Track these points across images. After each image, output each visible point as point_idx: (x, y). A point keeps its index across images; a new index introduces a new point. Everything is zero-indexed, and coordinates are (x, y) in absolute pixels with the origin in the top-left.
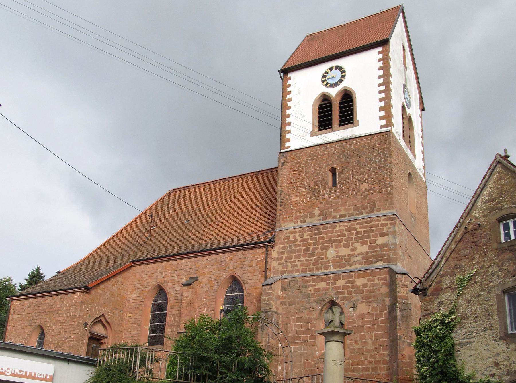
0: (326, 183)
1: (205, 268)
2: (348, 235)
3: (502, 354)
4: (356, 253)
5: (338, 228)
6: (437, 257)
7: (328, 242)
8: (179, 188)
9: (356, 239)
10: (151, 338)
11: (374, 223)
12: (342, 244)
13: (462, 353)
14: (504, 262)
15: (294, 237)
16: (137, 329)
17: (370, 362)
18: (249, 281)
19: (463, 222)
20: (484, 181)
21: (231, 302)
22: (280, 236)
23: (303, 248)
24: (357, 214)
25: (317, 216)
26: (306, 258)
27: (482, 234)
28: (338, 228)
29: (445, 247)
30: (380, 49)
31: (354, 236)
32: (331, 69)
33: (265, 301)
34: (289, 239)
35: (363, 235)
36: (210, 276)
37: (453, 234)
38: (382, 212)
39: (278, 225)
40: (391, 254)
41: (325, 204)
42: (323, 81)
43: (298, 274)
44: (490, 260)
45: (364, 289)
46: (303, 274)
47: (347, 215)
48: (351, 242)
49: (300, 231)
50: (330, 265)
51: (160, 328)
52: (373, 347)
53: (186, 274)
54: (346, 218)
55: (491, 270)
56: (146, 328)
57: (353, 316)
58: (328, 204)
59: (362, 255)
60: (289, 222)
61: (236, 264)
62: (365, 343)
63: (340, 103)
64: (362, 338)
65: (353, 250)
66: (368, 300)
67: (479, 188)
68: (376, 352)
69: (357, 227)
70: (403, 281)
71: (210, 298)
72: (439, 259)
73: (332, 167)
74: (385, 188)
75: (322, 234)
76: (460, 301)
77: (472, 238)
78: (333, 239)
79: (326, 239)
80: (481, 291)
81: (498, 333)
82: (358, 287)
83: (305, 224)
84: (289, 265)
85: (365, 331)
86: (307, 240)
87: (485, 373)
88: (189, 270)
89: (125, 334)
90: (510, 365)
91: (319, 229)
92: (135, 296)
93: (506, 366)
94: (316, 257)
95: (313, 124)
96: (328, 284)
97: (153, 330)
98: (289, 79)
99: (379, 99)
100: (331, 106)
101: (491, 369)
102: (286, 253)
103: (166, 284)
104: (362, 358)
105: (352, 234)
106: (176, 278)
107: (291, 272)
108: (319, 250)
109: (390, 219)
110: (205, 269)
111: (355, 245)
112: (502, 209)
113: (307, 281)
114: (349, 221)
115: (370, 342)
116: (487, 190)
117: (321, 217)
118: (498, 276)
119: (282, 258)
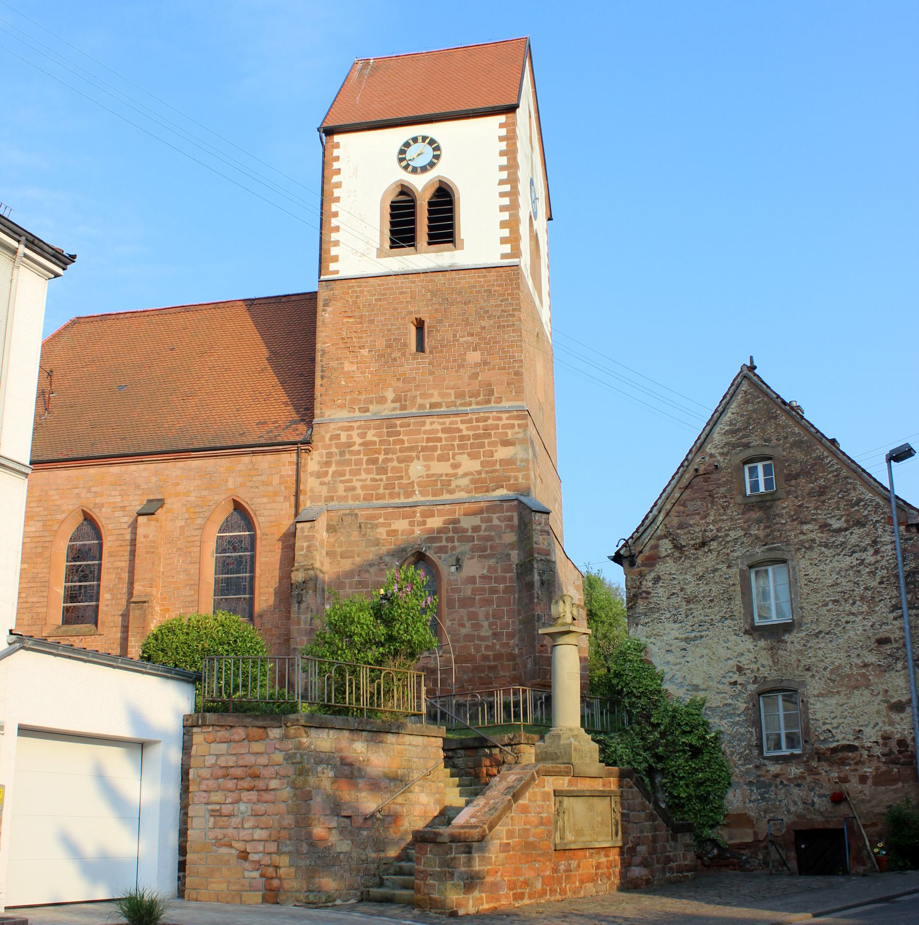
0: (405, 345)
1: (178, 484)
2: (447, 439)
3: (746, 654)
4: (460, 471)
5: (428, 427)
6: (652, 508)
7: (412, 449)
8: (89, 315)
9: (460, 447)
10: (66, 610)
11: (490, 422)
12: (436, 454)
13: (690, 653)
14: (752, 524)
15: (350, 437)
16: (41, 594)
17: (485, 658)
18: (266, 513)
19: (693, 459)
20: (724, 402)
21: (229, 548)
22: (323, 433)
23: (365, 458)
24: (462, 405)
25: (389, 401)
26: (372, 476)
27: (720, 480)
28: (428, 427)
29: (664, 495)
30: (502, 118)
31: (456, 443)
32: (415, 140)
33: (302, 550)
34: (340, 439)
35: (472, 441)
36: (189, 499)
37: (677, 476)
38: (505, 404)
39: (317, 412)
40: (520, 476)
41: (404, 382)
42: (401, 160)
43: (357, 502)
44: (732, 519)
45: (475, 535)
46: (366, 504)
47: (444, 405)
48: (451, 453)
49: (359, 428)
50: (415, 491)
51: (85, 592)
52: (491, 632)
53: (139, 492)
54: (443, 409)
55: (733, 534)
57: (456, 580)
58: (409, 383)
59: (471, 477)
60: (338, 409)
61: (240, 480)
62: (477, 626)
63: (430, 204)
64: (473, 616)
65: (456, 466)
66: (481, 552)
67: (716, 411)
68: (495, 641)
69: (462, 426)
70: (543, 525)
71: (189, 539)
72: (655, 512)
73: (418, 316)
74: (510, 363)
75: (399, 435)
76: (688, 577)
77: (705, 484)
78: (420, 444)
79: (406, 445)
80: (718, 564)
81: (742, 624)
82: (466, 530)
83: (368, 414)
84: (341, 487)
85: (477, 605)
86: (374, 443)
87: (724, 680)
88: (144, 486)
90: (758, 669)
91: (395, 426)
92: (33, 529)
93: (752, 671)
94: (390, 474)
95: (382, 232)
96: (412, 524)
97: (71, 596)
98: (337, 146)
99: (500, 206)
100: (414, 207)
101: (731, 674)
102: (334, 465)
104: (472, 650)
105: (454, 439)
106: (118, 499)
107: (345, 498)
108: (395, 463)
109: (517, 418)
110: (178, 485)
111: (458, 458)
112: (750, 447)
113: (375, 517)
114: (447, 415)
115: (486, 624)
116: (728, 416)
117: (398, 405)
118: (743, 543)
119: (326, 473)
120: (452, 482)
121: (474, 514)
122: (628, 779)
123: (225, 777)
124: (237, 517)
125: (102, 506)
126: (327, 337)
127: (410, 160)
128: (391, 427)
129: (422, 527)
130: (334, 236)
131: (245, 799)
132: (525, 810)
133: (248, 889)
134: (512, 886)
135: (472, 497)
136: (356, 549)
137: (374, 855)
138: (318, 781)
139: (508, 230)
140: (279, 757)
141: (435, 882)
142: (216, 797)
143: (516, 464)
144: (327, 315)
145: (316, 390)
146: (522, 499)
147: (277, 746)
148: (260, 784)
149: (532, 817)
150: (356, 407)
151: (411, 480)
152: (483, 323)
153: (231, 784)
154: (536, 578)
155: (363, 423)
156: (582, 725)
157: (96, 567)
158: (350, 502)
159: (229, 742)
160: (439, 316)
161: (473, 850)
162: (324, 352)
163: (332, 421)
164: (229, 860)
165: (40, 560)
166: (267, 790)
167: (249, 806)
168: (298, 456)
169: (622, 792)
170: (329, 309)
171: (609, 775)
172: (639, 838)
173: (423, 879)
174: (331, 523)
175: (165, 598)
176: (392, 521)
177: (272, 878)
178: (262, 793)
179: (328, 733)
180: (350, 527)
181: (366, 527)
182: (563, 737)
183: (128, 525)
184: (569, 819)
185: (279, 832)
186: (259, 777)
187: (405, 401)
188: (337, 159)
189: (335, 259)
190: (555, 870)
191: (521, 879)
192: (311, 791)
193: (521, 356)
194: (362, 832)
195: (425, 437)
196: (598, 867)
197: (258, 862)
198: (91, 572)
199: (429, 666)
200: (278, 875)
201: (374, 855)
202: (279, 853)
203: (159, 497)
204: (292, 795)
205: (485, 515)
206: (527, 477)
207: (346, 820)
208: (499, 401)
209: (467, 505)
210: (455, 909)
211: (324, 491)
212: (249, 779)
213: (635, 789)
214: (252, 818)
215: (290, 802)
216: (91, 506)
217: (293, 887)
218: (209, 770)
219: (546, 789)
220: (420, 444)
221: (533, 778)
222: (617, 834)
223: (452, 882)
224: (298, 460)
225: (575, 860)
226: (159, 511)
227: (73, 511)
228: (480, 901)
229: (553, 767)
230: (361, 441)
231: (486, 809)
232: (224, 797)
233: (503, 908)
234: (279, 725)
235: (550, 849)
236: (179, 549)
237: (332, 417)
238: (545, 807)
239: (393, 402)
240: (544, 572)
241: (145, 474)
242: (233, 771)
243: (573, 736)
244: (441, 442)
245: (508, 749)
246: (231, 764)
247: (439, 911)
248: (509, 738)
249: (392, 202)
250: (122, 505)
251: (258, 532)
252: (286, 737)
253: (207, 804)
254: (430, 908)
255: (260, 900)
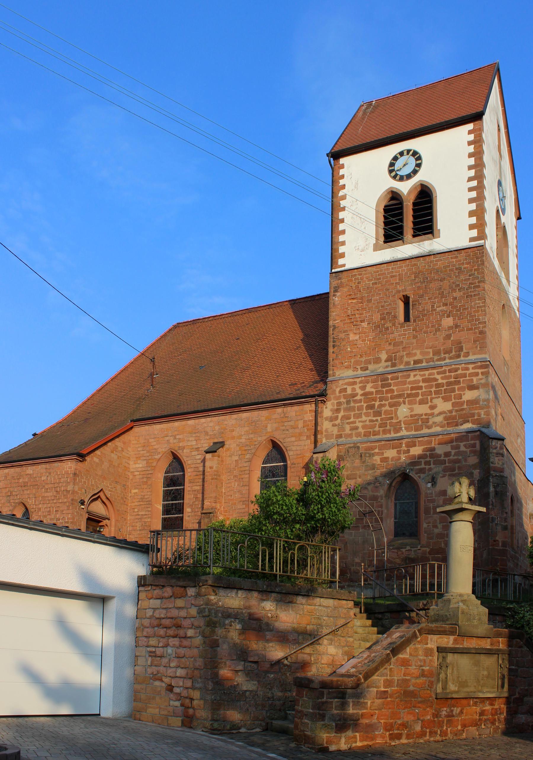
0: (395, 317)
4: (436, 411)
5: (412, 379)
7: (400, 396)
8: (185, 321)
9: (436, 393)
10: (164, 520)
11: (460, 372)
12: (418, 399)
15: (354, 389)
18: (294, 448)
22: (334, 388)
23: (365, 405)
24: (438, 360)
25: (383, 361)
26: (370, 418)
28: (412, 379)
30: (470, 126)
31: (433, 390)
32: (401, 154)
34: (346, 392)
35: (445, 387)
36: (241, 441)
38: (472, 357)
39: (330, 372)
40: (483, 413)
42: (390, 172)
43: (359, 438)
45: (447, 459)
46: (366, 439)
47: (424, 361)
48: (429, 397)
50: (402, 428)
51: (176, 507)
53: (208, 438)
54: (423, 364)
56: (158, 507)
57: (432, 494)
58: (398, 346)
59: (444, 415)
61: (275, 425)
63: (414, 204)
65: (433, 407)
69: (438, 377)
70: (498, 449)
71: (242, 469)
73: (404, 294)
75: (390, 386)
78: (406, 392)
79: (396, 393)
82: (440, 456)
83: (367, 372)
84: (347, 427)
86: (372, 393)
88: (211, 433)
89: (131, 515)
91: (387, 379)
92: (141, 466)
94: (383, 416)
96: (399, 452)
97: (167, 510)
98: (342, 166)
102: (342, 411)
103: (181, 451)
104: (443, 545)
105: (431, 387)
107: (350, 436)
108: (387, 408)
109: (481, 367)
110: (234, 431)
111: (435, 401)
114: (426, 369)
117: (389, 363)
120: (430, 420)
121: (446, 443)
122: (518, 640)
123: (159, 626)
124: (275, 453)
125: (184, 448)
126: (336, 315)
127: (398, 170)
128: (384, 381)
129: (406, 455)
130: (341, 238)
131: (171, 644)
132: (405, 663)
133: (172, 714)
134: (388, 727)
135: (445, 431)
136: (358, 472)
137: (280, 694)
138: (226, 631)
139: (475, 218)
140: (193, 611)
141: (308, 722)
142: (153, 642)
143: (479, 404)
144: (337, 299)
145: (329, 356)
146: (484, 430)
147: (193, 602)
148: (181, 632)
149: (413, 669)
150: (359, 367)
151: (399, 419)
152: (455, 295)
153: (162, 632)
154: (492, 489)
155: (363, 378)
156: (474, 592)
157: (182, 490)
158: (354, 438)
159: (161, 598)
160: (421, 292)
161: (347, 696)
162: (335, 327)
163: (341, 379)
164: (160, 691)
165: (145, 486)
166: (185, 637)
167: (174, 649)
168: (316, 406)
169: (510, 651)
170: (338, 294)
171: (499, 635)
172: (527, 690)
173: (299, 718)
174: (340, 454)
175: (226, 511)
176: (384, 451)
177: (188, 708)
178: (182, 639)
179: (237, 593)
180: (354, 456)
181: (365, 457)
182: (453, 601)
183: (201, 461)
184: (453, 672)
185: (193, 672)
186: (180, 627)
187: (395, 360)
188: (343, 177)
189: (343, 255)
190: (436, 715)
191: (399, 722)
192: (218, 640)
193: (485, 318)
194: (269, 675)
195: (410, 386)
196: (482, 713)
197: (179, 694)
198: (179, 494)
199: (410, 556)
200: (193, 706)
201: (280, 694)
202: (193, 688)
203: (221, 440)
204: (202, 642)
205: (454, 444)
206: (488, 414)
207: (253, 665)
208: (467, 354)
209: (440, 437)
210: (325, 745)
211: (335, 431)
212: (174, 628)
213: (525, 648)
214: (176, 659)
215: (201, 648)
216: (177, 449)
217: (202, 716)
218: (148, 621)
219: (429, 646)
220: (406, 392)
221: (414, 636)
222: (503, 686)
223: (322, 723)
224: (316, 409)
225: (458, 707)
226: (220, 450)
227: (165, 452)
228: (353, 740)
229: (437, 627)
230: (363, 392)
231: (366, 661)
232: (157, 642)
233: (377, 746)
234: (193, 584)
235: (432, 697)
236: (235, 476)
237: (341, 375)
238: (428, 661)
239: (386, 361)
240: (498, 485)
241: (211, 424)
242: (163, 621)
243: (462, 601)
244: (422, 389)
245: (422, 613)
246: (162, 616)
247: (310, 746)
248: (423, 604)
249: (385, 206)
250: (196, 447)
251: (289, 462)
252: (198, 595)
253: (147, 646)
254: (305, 743)
255: (180, 724)
